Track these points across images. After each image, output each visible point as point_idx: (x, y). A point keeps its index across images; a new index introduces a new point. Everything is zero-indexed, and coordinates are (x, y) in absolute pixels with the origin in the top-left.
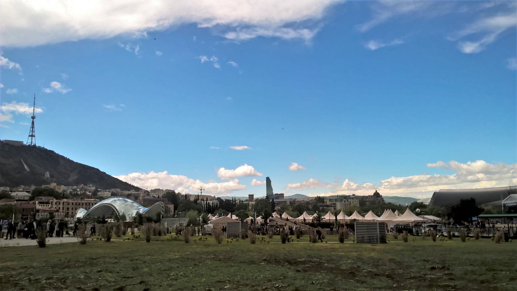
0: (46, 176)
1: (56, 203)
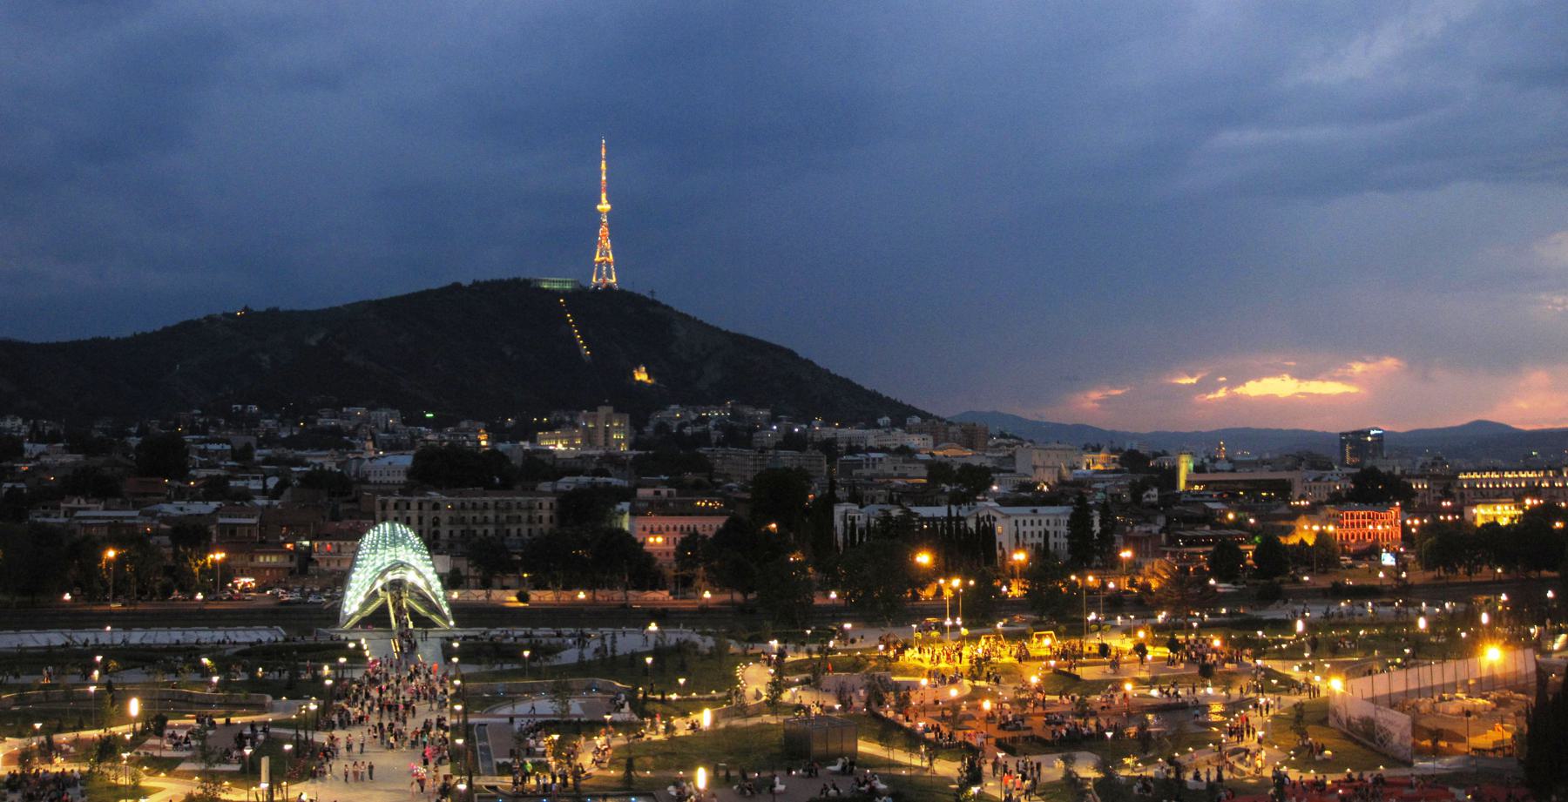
1: (396, 506)
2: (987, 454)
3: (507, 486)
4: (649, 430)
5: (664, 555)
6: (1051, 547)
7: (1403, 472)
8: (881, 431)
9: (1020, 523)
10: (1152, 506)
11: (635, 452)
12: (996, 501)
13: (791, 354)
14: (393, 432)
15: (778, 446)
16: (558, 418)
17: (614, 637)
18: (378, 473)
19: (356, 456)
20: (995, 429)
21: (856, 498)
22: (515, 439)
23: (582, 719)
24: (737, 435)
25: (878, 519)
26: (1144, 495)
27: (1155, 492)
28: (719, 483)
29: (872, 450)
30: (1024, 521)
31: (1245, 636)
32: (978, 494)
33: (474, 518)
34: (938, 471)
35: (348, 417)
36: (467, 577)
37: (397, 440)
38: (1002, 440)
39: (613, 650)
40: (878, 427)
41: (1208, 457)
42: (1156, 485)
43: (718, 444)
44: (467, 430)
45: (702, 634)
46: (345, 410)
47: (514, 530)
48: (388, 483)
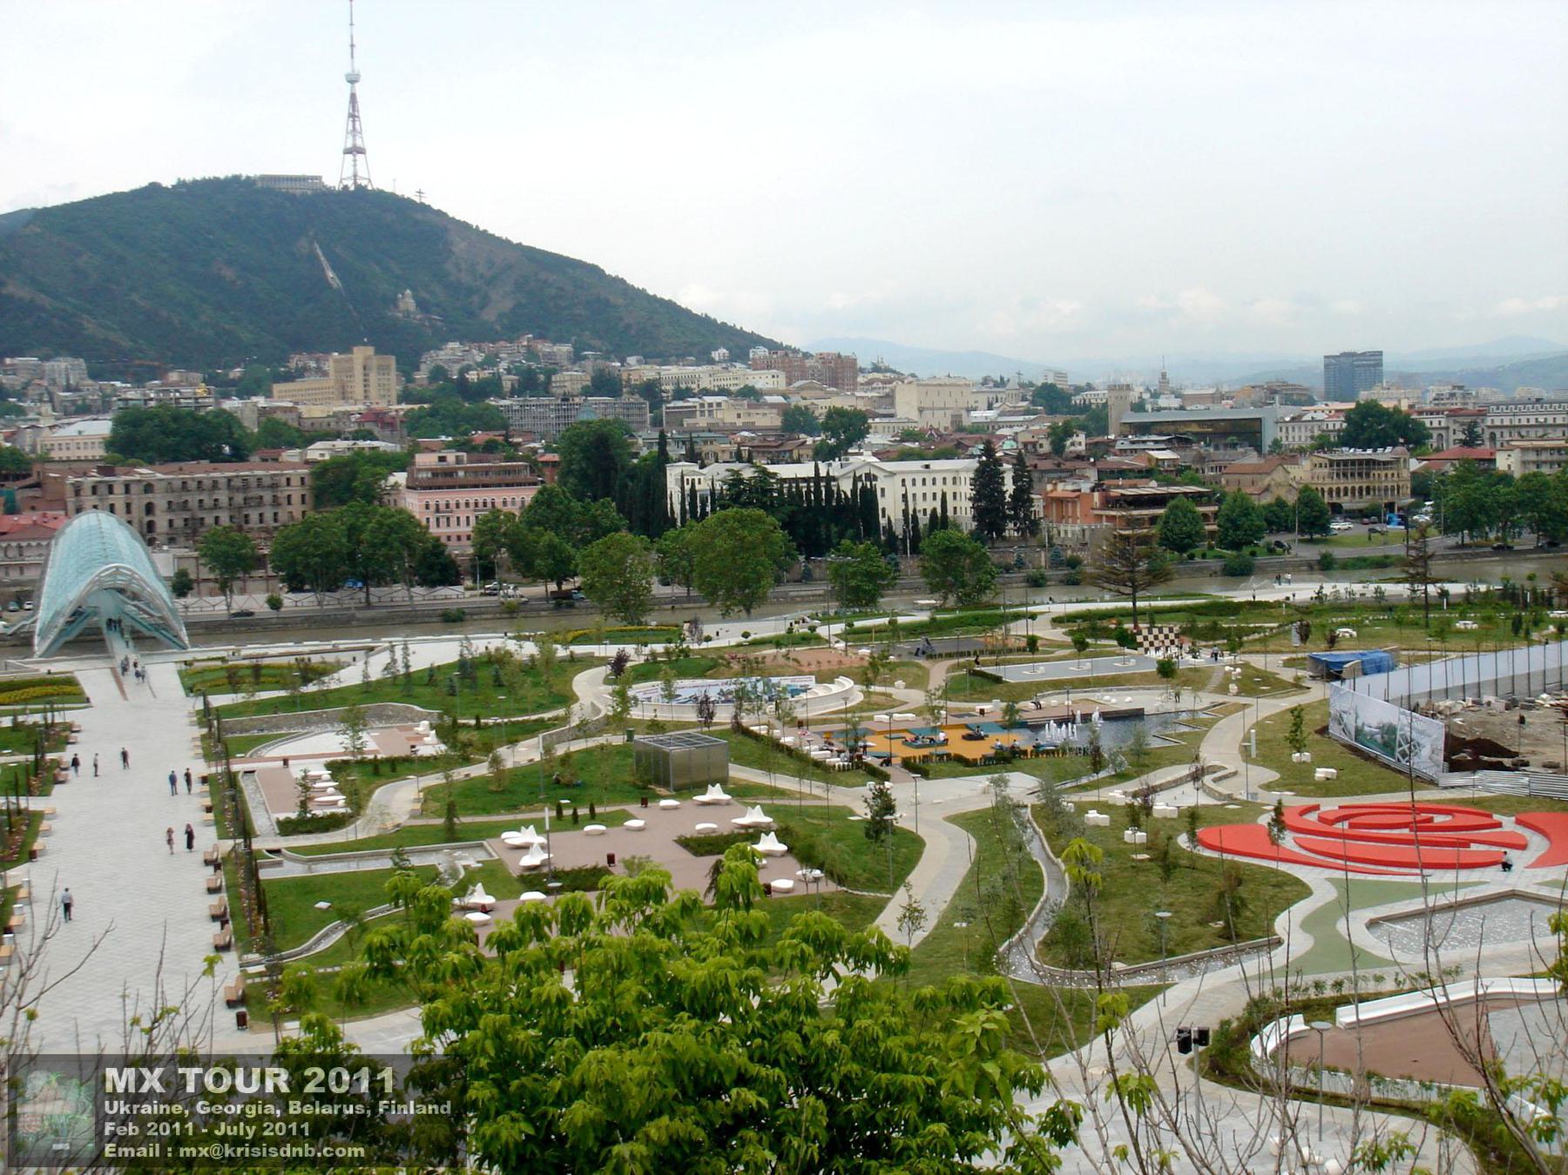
0: (402, 306)
1: (94, 490)
2: (857, 394)
3: (239, 456)
4: (421, 376)
5: (454, 538)
6: (950, 513)
7: (1411, 407)
8: (718, 368)
9: (909, 483)
10: (1079, 457)
11: (405, 406)
12: (874, 454)
13: (594, 271)
14: (76, 389)
15: (586, 392)
16: (300, 365)
17: (406, 648)
18: (64, 447)
19: (30, 423)
20: (864, 362)
21: (693, 456)
22: (245, 393)
23: (379, 757)
24: (531, 384)
25: (724, 482)
26: (1068, 443)
27: (1081, 438)
28: (519, 444)
29: (707, 392)
30: (914, 480)
31: (1215, 623)
32: (850, 445)
33: (201, 501)
34: (796, 420)
35: (14, 370)
36: (198, 581)
37: (84, 400)
38: (876, 375)
39: (407, 666)
40: (712, 362)
41: (1148, 390)
42: (1083, 428)
43: (513, 393)
44: (178, 384)
45: (518, 638)
46: (8, 361)
47: (254, 516)
48: (79, 460)
